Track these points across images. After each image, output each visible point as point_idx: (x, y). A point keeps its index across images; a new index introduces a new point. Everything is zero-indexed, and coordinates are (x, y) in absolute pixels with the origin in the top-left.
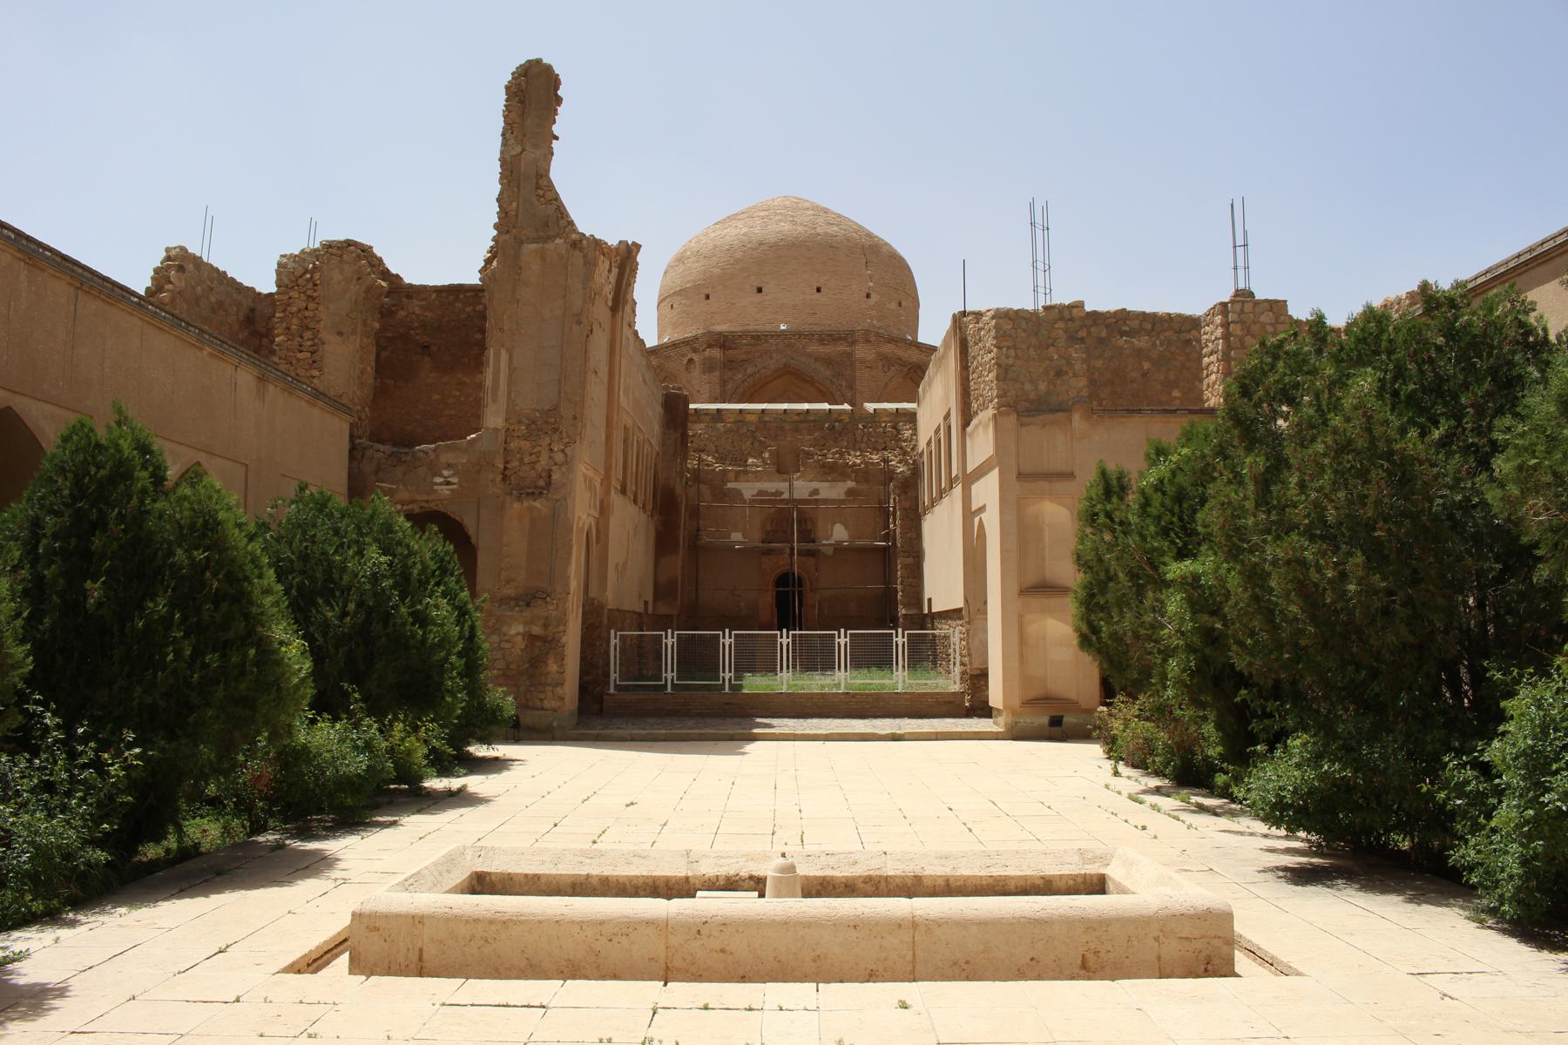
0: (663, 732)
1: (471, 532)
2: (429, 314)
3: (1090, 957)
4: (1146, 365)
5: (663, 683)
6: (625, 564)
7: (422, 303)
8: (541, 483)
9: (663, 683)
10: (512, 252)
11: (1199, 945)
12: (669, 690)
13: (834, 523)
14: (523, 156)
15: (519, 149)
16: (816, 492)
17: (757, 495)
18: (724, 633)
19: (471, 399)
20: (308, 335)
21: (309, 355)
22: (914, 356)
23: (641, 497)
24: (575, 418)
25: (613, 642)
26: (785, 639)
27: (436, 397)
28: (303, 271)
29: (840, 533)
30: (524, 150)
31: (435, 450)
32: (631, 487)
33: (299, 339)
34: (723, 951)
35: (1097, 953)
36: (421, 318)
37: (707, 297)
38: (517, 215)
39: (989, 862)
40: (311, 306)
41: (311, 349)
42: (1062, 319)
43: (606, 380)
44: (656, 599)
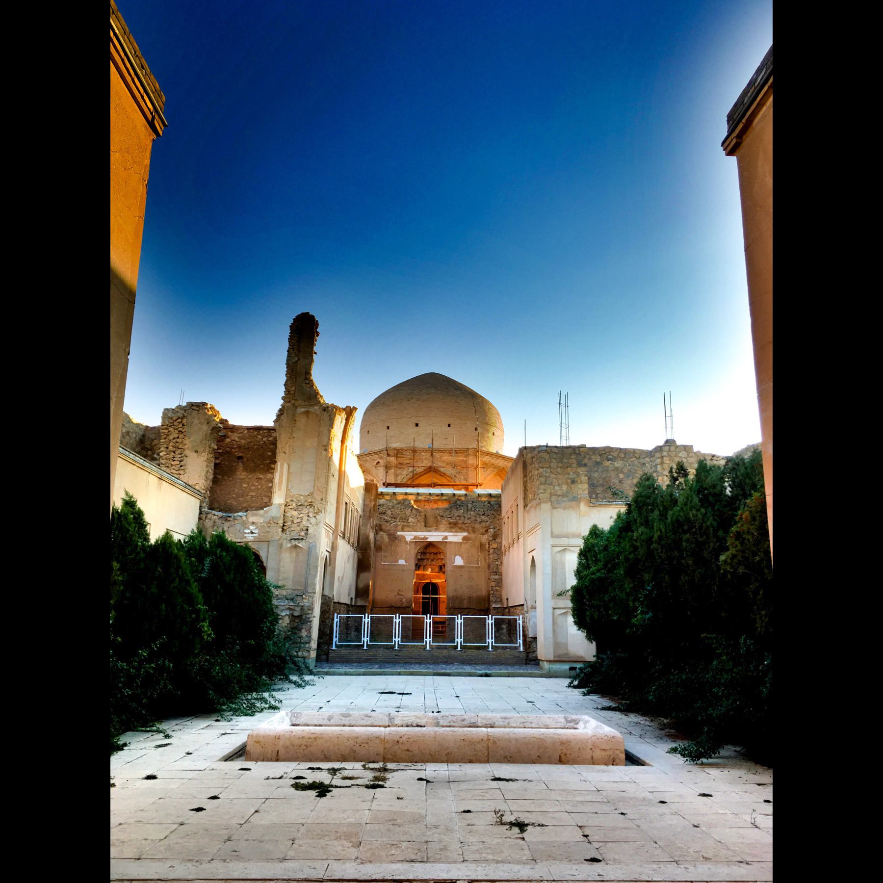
0: (363, 670)
1: (264, 559)
2: (243, 441)
3: (563, 757)
4: (621, 476)
5: (362, 643)
6: (343, 577)
7: (240, 435)
8: (303, 533)
9: (362, 643)
10: (292, 412)
11: (610, 753)
12: (365, 648)
13: (456, 555)
14: (298, 362)
15: (296, 359)
16: (446, 538)
17: (414, 539)
18: (427, 617)
19: (264, 487)
20: (178, 451)
21: (178, 462)
22: (501, 463)
23: (352, 540)
24: (322, 500)
25: (336, 620)
26: (428, 620)
27: (244, 485)
28: (177, 418)
29: (459, 561)
30: (299, 359)
31: (246, 516)
32: (347, 535)
33: (173, 454)
34: (408, 750)
35: (566, 754)
36: (239, 443)
37: (388, 428)
38: (294, 393)
39: (524, 721)
40: (181, 436)
41: (180, 459)
42: (575, 453)
43: (337, 480)
44: (356, 597)
